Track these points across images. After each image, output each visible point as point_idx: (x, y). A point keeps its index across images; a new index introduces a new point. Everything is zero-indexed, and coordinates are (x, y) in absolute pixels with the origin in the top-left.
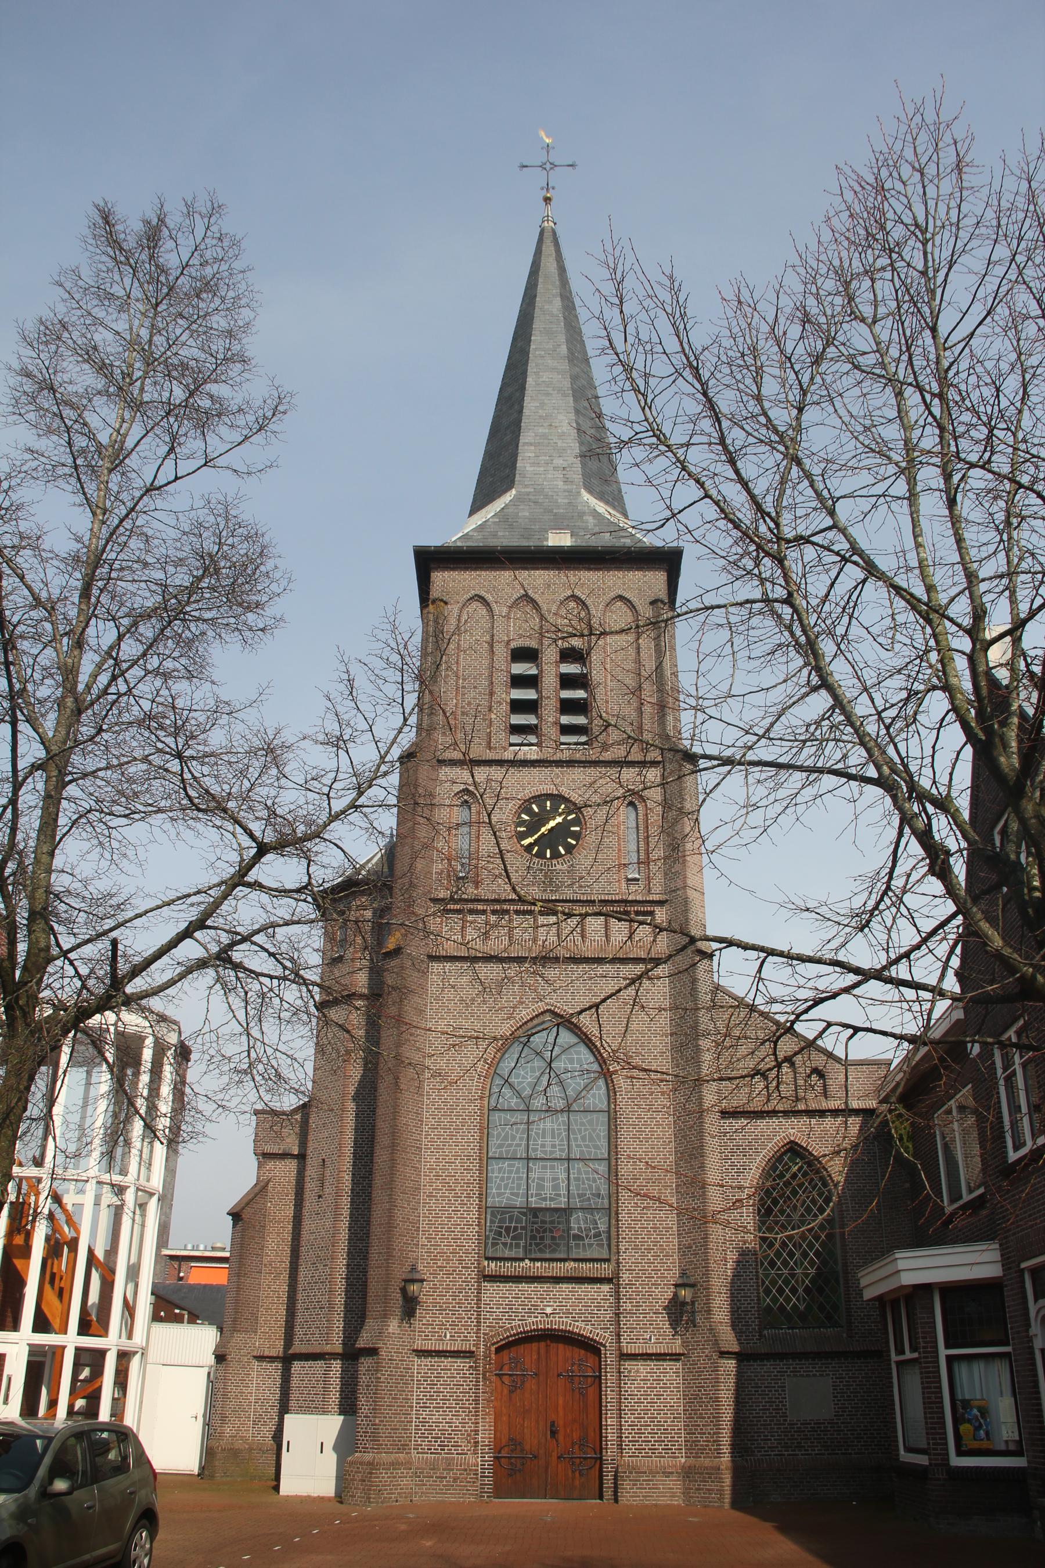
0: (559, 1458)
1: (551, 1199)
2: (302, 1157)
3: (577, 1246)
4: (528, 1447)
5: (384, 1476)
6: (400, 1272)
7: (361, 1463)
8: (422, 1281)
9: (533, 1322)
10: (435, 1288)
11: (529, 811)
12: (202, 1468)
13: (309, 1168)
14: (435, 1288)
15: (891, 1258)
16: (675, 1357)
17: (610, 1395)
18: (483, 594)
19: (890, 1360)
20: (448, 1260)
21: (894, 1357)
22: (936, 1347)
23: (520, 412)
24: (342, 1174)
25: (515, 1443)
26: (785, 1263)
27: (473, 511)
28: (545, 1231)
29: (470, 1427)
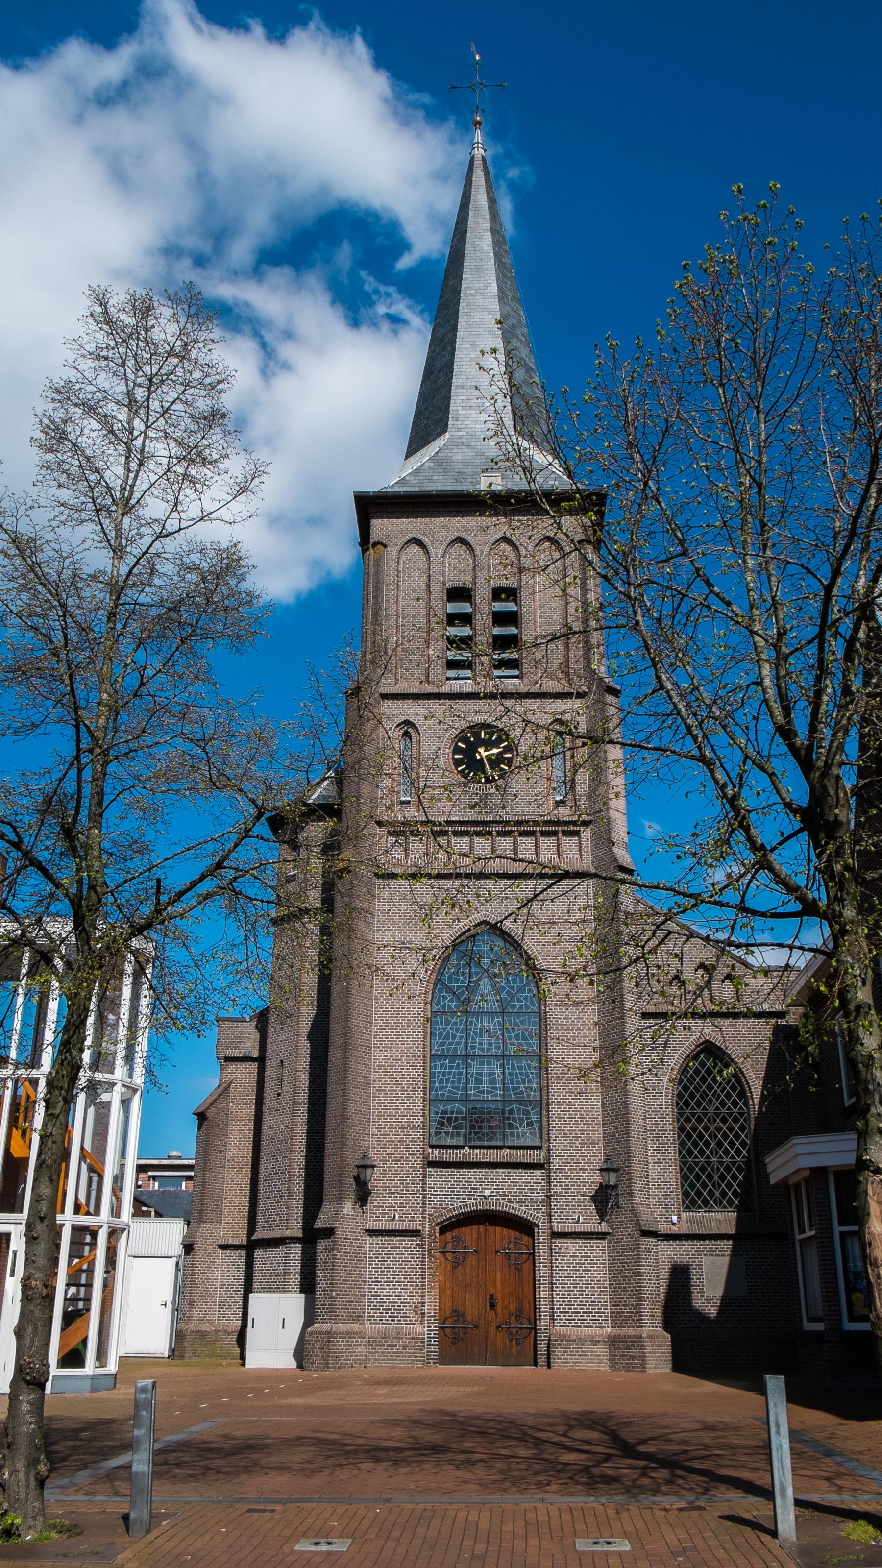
0: (497, 1328)
1: (488, 1092)
2: (261, 1060)
3: (512, 1134)
4: (469, 1318)
5: (340, 1344)
6: (352, 1159)
7: (320, 1333)
8: (373, 1166)
9: (474, 1204)
10: (384, 1174)
11: (465, 740)
12: (172, 1351)
13: (268, 1068)
14: (384, 1174)
15: (791, 1144)
16: (602, 1236)
17: (542, 1270)
18: (420, 536)
20: (396, 1148)
21: (798, 1237)
22: (831, 1225)
23: (453, 355)
24: (299, 1073)
25: (458, 1314)
26: (701, 1152)
27: (409, 454)
28: (483, 1121)
29: (417, 1299)
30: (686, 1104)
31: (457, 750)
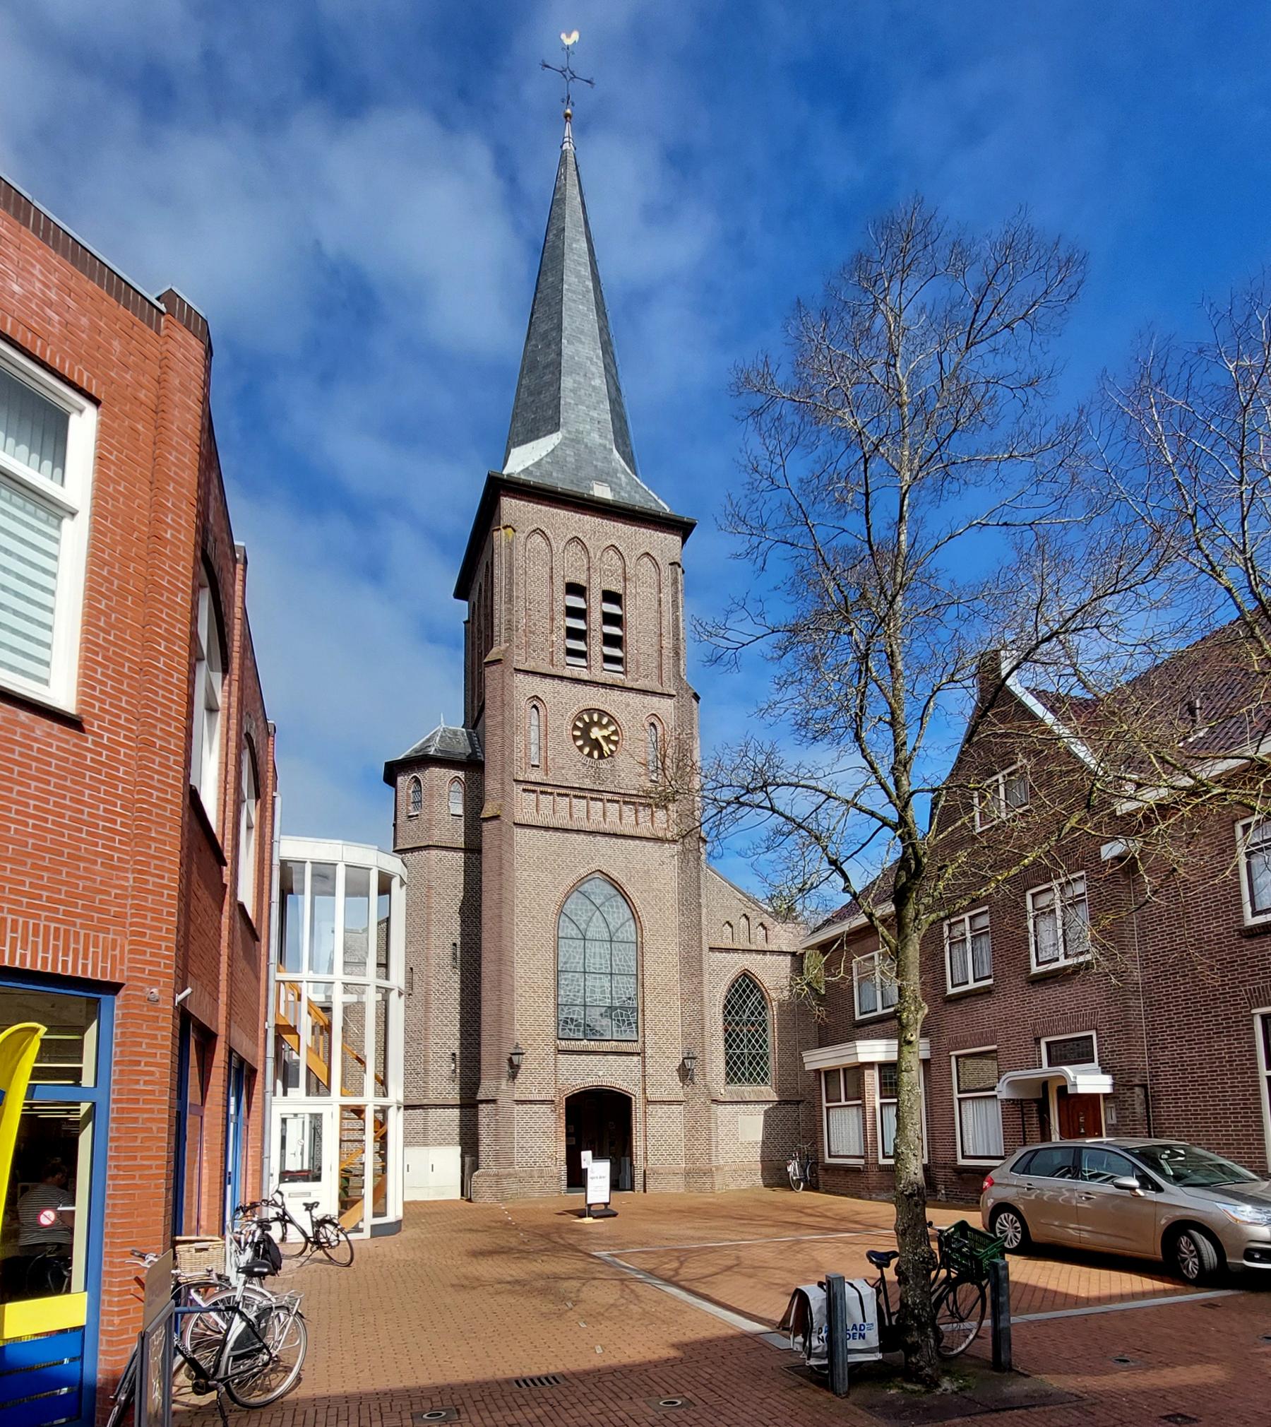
6: (508, 1049)
16: (679, 1103)
19: (821, 1106)
26: (738, 1046)
30: (729, 1013)
31: (575, 727)
